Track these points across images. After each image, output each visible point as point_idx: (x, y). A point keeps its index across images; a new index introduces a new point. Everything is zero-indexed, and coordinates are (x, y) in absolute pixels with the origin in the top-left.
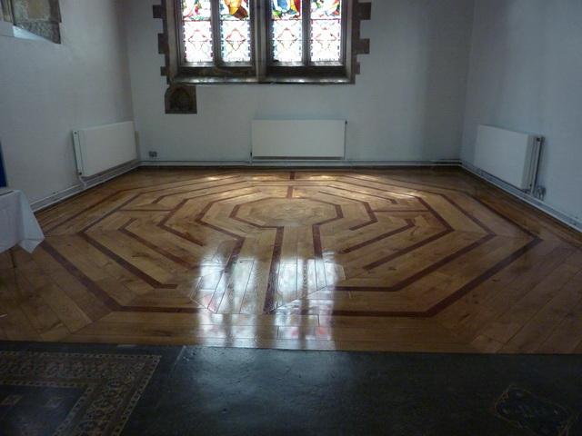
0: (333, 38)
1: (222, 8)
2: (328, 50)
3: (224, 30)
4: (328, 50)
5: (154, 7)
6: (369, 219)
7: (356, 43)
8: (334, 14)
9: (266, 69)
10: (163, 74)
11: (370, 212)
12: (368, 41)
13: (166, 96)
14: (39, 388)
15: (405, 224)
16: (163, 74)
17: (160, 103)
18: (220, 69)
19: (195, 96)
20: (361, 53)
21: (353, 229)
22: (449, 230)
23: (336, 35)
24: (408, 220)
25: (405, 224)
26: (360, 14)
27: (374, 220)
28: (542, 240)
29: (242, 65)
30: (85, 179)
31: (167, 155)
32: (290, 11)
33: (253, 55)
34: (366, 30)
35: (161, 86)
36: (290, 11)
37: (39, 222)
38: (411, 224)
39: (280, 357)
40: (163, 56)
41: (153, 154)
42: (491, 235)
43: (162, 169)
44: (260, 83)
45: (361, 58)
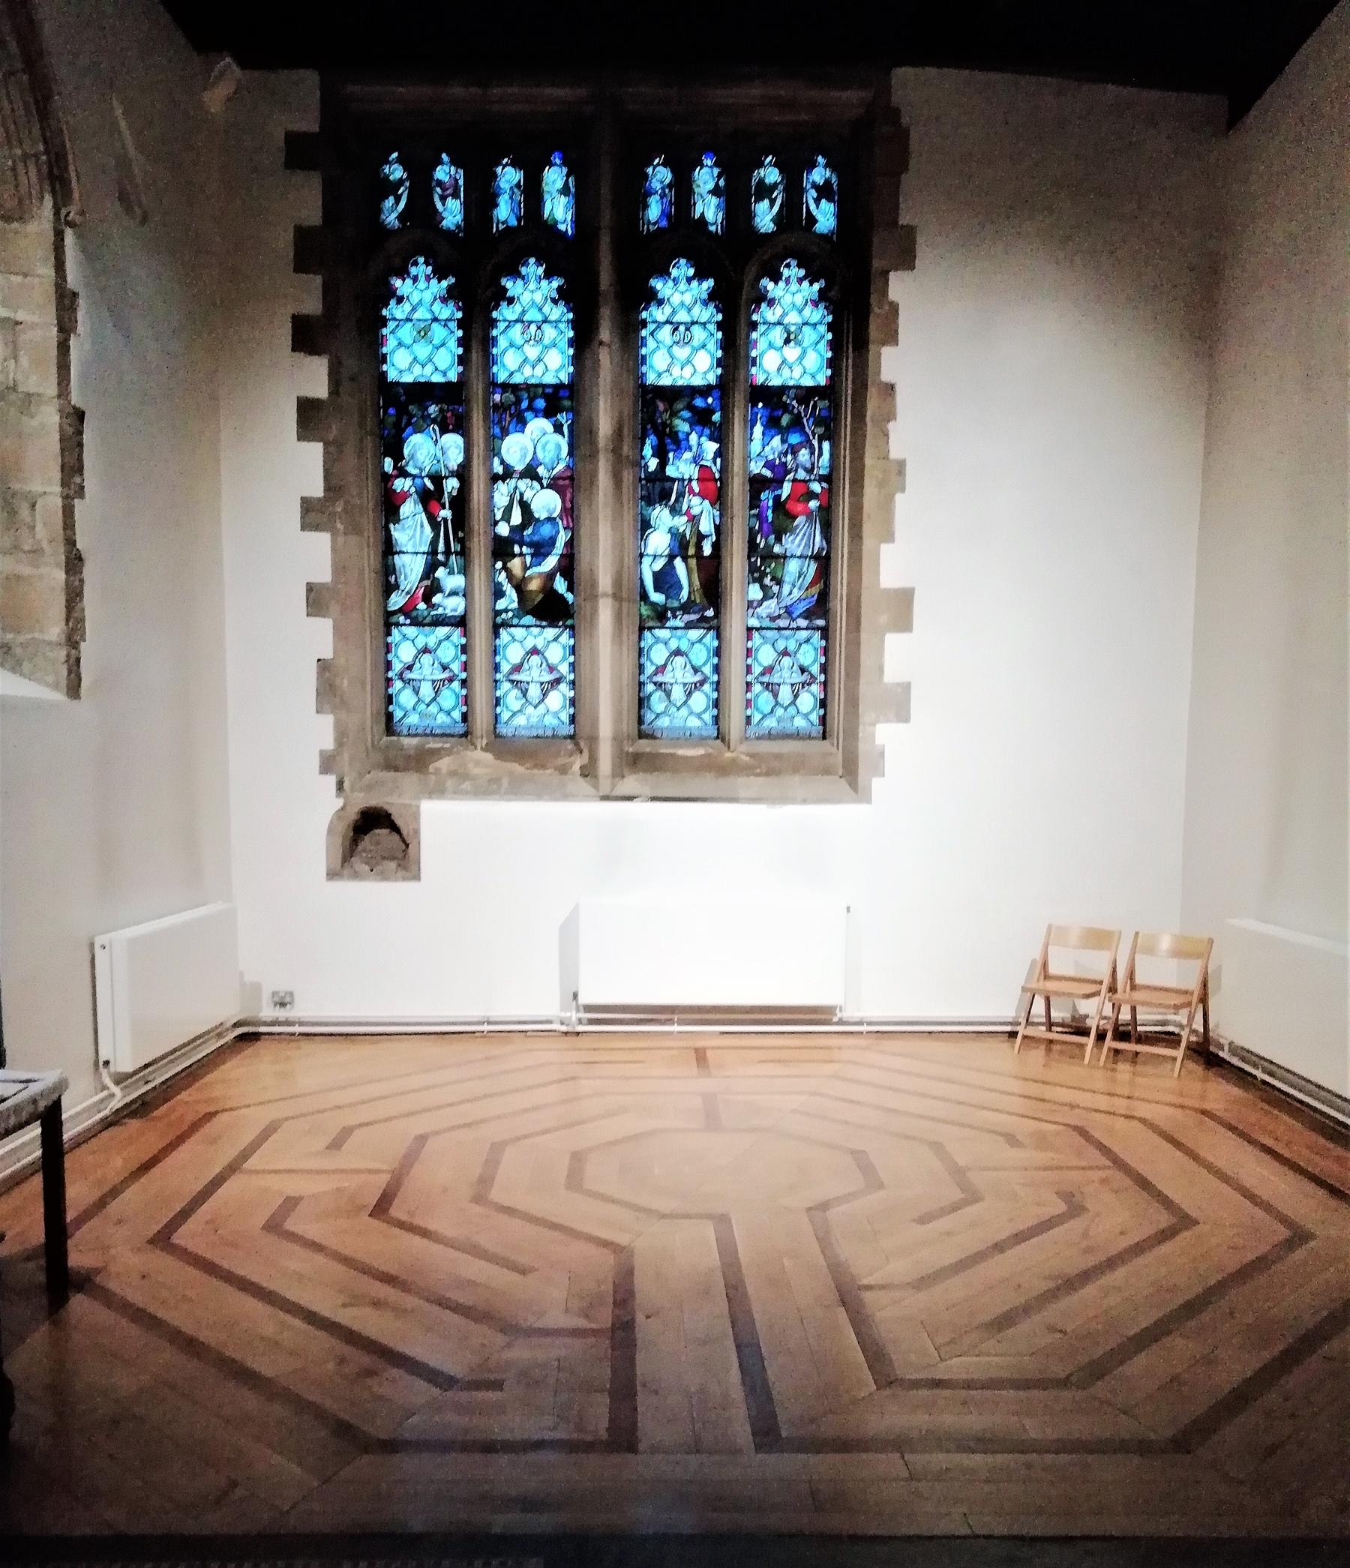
0: (805, 677)
5: (310, 588)
6: (958, 1195)
11: (958, 1173)
12: (907, 687)
14: (47, 152)
15: (1061, 1207)
20: (888, 721)
21: (923, 1220)
22: (1184, 1221)
24: (1068, 1197)
25: (1061, 1207)
27: (972, 1197)
30: (120, 1079)
32: (686, 608)
33: (882, 641)
36: (686, 608)
37: (62, 450)
38: (1075, 1208)
42: (1299, 1237)
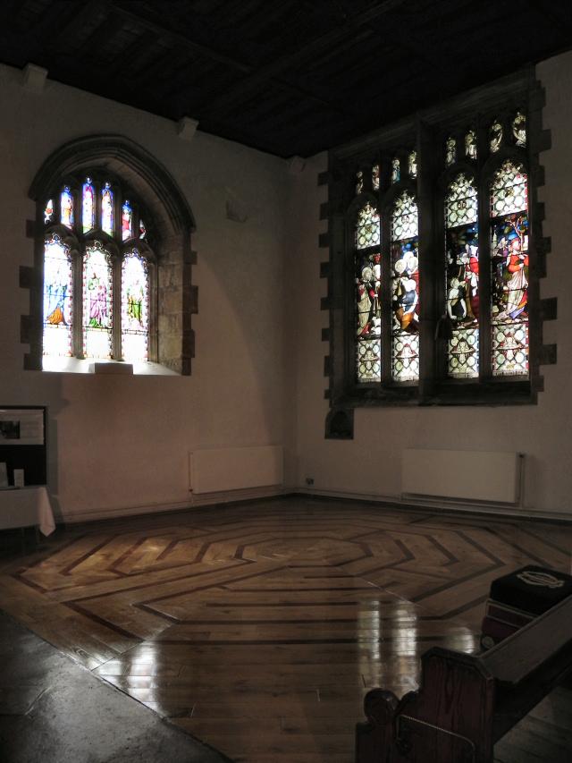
1: (394, 324)
2: (514, 362)
3: (126, 355)
4: (514, 362)
7: (540, 352)
8: (520, 316)
9: (439, 384)
10: (326, 397)
12: (555, 346)
13: (327, 420)
16: (326, 397)
17: (321, 427)
18: (391, 391)
19: (353, 421)
20: (545, 364)
23: (524, 342)
26: (542, 314)
28: (19, 423)
29: (410, 384)
31: (329, 483)
34: (550, 331)
35: (322, 409)
36: (467, 319)
39: (80, 552)
40: (327, 378)
41: (310, 482)
43: (315, 497)
44: (421, 405)
45: (544, 370)
